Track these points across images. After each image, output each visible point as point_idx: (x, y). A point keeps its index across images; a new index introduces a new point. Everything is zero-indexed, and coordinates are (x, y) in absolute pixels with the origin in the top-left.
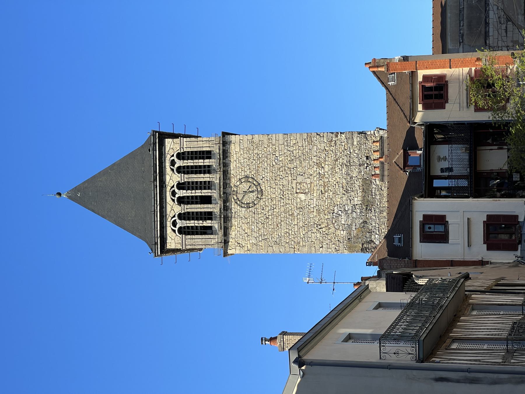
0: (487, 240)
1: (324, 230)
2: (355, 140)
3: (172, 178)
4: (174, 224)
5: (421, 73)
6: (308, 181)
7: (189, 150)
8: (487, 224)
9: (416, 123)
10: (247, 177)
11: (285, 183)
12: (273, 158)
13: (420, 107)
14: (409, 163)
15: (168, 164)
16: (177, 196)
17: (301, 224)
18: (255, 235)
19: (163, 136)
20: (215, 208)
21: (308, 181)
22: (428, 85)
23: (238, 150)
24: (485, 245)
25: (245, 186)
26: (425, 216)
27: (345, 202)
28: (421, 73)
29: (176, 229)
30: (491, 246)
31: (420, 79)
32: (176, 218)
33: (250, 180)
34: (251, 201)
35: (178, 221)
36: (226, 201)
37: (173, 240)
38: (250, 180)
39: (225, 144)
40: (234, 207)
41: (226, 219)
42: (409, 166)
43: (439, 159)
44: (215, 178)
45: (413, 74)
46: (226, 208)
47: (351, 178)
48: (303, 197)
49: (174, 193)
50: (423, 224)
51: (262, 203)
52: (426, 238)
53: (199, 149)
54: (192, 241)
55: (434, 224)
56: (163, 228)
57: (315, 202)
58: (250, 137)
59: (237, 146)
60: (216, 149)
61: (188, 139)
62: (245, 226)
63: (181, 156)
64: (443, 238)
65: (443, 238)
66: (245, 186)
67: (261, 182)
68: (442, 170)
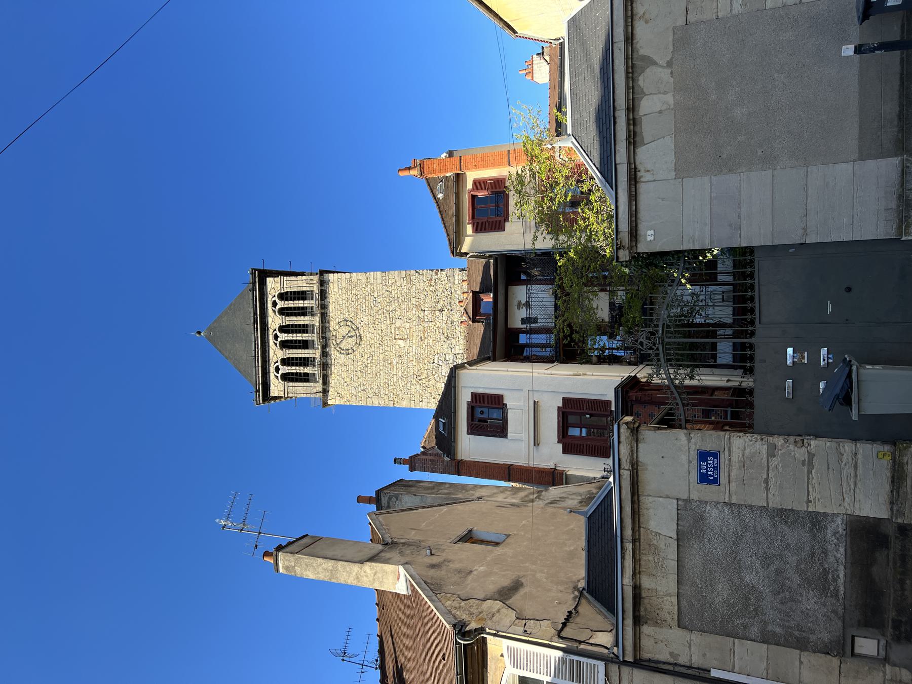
0: (563, 437)
1: (424, 381)
2: (456, 278)
3: (275, 321)
4: (277, 369)
5: (471, 176)
6: (407, 325)
7: (289, 290)
8: (563, 413)
9: (466, 254)
10: (346, 320)
11: (384, 327)
12: (371, 299)
13: (469, 229)
14: (481, 311)
15: (270, 305)
16: (279, 339)
17: (400, 374)
18: (354, 384)
19: (264, 275)
20: (314, 353)
21: (407, 325)
22: (481, 194)
23: (336, 290)
24: (560, 445)
25: (344, 331)
26: (474, 396)
27: (446, 350)
28: (471, 176)
29: (279, 375)
30: (570, 446)
31: (469, 185)
32: (279, 363)
33: (349, 323)
34: (349, 347)
35: (280, 367)
36: (325, 347)
37: (277, 387)
38: (349, 323)
39: (322, 283)
40: (334, 353)
41: (325, 366)
42: (481, 315)
43: (520, 305)
44: (316, 321)
45: (459, 178)
46: (325, 354)
47: (452, 322)
48: (401, 343)
49: (276, 337)
50: (471, 409)
51: (361, 349)
52: (478, 427)
53: (299, 289)
54: (293, 389)
55: (489, 408)
56: (265, 373)
57: (414, 350)
58: (348, 275)
59: (336, 285)
60: (316, 289)
61: (288, 278)
62: (344, 375)
63: (283, 296)
64: (500, 431)
65: (500, 431)
66: (344, 331)
67: (359, 326)
68: (524, 321)
